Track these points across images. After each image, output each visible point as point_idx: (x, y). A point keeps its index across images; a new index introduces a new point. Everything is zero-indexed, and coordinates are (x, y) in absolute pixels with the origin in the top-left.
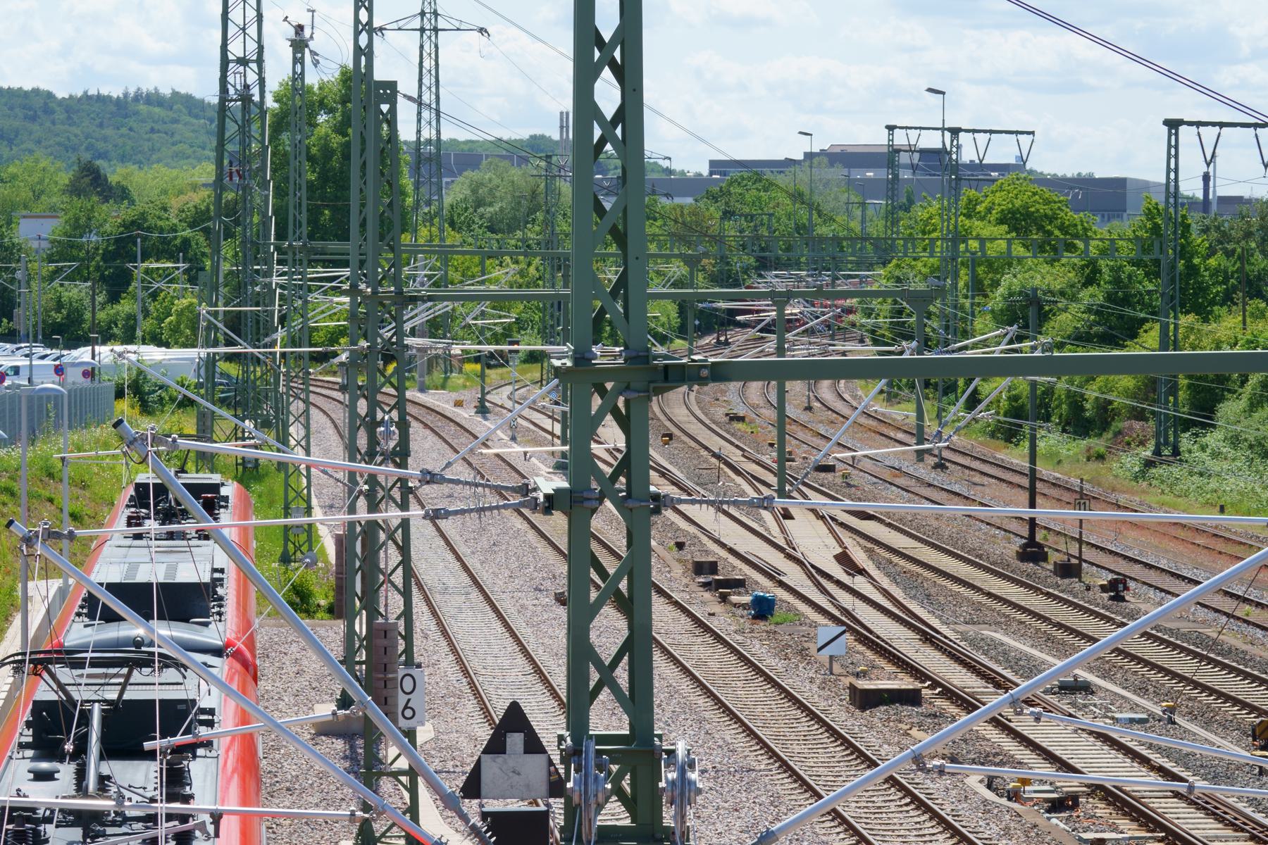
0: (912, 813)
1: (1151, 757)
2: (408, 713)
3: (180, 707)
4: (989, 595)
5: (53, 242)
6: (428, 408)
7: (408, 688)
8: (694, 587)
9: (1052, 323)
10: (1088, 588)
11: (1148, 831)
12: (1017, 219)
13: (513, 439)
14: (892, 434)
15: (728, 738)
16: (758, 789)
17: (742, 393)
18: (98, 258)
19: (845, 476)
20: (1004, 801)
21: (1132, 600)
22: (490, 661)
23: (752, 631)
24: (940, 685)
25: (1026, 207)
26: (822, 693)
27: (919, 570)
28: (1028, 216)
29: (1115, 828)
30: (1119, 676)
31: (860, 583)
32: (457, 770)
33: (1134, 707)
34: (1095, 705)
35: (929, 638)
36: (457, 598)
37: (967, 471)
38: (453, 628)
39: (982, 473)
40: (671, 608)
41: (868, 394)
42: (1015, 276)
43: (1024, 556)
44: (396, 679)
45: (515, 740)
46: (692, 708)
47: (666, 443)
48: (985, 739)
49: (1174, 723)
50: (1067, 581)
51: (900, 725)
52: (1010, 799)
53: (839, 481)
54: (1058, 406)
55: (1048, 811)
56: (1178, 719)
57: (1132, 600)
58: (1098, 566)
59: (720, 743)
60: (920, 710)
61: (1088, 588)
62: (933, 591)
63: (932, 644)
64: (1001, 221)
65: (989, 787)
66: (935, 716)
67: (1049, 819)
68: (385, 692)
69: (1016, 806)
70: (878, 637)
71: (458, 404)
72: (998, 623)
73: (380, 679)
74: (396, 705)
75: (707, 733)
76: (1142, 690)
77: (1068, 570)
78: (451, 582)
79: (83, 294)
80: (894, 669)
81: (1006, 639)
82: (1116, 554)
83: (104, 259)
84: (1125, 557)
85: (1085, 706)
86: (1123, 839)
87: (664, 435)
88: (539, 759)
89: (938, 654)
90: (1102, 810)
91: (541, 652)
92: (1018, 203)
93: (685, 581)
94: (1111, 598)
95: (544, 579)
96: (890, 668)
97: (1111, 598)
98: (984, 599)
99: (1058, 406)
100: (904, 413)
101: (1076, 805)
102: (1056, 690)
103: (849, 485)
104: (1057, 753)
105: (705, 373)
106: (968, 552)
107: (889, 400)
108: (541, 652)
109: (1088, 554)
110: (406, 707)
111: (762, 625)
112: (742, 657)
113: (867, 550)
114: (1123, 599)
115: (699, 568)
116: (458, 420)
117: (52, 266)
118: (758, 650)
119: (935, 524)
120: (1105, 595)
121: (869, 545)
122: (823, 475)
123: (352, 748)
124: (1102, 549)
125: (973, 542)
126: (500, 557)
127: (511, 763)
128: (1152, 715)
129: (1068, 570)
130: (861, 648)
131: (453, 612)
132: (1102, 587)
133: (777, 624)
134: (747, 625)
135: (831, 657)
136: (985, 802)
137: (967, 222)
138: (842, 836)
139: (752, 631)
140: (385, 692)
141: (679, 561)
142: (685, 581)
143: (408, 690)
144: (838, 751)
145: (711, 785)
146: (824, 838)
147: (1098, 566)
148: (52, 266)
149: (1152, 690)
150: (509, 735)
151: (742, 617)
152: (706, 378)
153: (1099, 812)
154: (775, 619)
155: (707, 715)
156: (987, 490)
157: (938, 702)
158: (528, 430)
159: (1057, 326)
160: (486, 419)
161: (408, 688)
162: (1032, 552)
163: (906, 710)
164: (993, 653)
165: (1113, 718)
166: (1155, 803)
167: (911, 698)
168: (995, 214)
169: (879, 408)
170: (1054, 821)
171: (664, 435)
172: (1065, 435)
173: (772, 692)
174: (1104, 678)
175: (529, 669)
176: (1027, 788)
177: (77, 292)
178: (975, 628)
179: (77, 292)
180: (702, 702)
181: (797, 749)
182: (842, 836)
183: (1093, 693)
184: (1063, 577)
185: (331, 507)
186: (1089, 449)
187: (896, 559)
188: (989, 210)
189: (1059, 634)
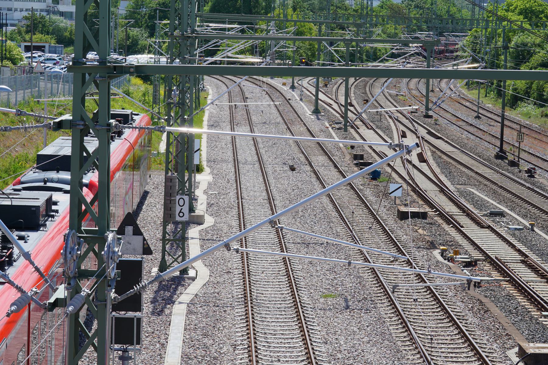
0: (404, 265)
1: (516, 245)
2: (181, 214)
3: (33, 209)
4: (476, 173)
5: (127, 11)
6: (271, 86)
7: (181, 204)
8: (352, 165)
9: (533, 58)
10: (520, 172)
11: (503, 277)
12: (527, 13)
13: (301, 100)
14: (464, 103)
15: (338, 230)
16: (342, 252)
17: (447, 84)
18: (147, 17)
19: (436, 120)
20: (446, 262)
21: (538, 177)
22: (252, 193)
23: (369, 185)
24: (439, 211)
25: (531, 7)
26: (387, 212)
27: (452, 161)
28: (532, 12)
29: (489, 275)
30: (518, 209)
31: (423, 167)
32: (217, 239)
33: (519, 223)
34: (503, 222)
35: (443, 190)
36: (249, 166)
37: (490, 120)
38: (243, 179)
39: (495, 121)
40: (338, 173)
41: (459, 84)
42: (519, 37)
43: (498, 157)
44: (175, 200)
45: (129, 229)
46: (328, 216)
47: (365, 104)
48: (449, 235)
49: (534, 231)
50: (513, 168)
51: (415, 227)
52: (449, 261)
53: (433, 122)
54: (533, 93)
55: (464, 267)
56: (535, 229)
57: (538, 177)
58: (528, 162)
59: (334, 232)
60: (425, 221)
61: (520, 172)
62: (453, 170)
63: (444, 193)
64: (520, 14)
65: (442, 256)
66: (431, 224)
67: (463, 270)
68: (170, 205)
69: (450, 264)
70: (420, 189)
71: (284, 84)
72: (475, 185)
73: (168, 200)
74: (175, 211)
75: (331, 228)
76: (524, 216)
77: (513, 164)
78: (249, 159)
79: (138, 33)
80: (423, 203)
81: (475, 192)
82: (539, 157)
83: (149, 18)
84: (542, 159)
85: (498, 222)
86: (491, 280)
87: (365, 100)
88: (140, 238)
89: (444, 197)
90: (487, 267)
91: (274, 190)
92: (528, 6)
93: (349, 162)
94: (529, 176)
95: (289, 159)
96: (421, 202)
97: (529, 176)
98: (473, 174)
99: (533, 93)
100: (472, 94)
101: (476, 265)
102: (489, 214)
103: (436, 124)
104: (476, 242)
105: (132, 70)
106: (475, 155)
107: (468, 88)
108: (274, 190)
109: (523, 155)
110: (180, 212)
111: (374, 182)
112: (359, 196)
113: (433, 153)
114: (533, 177)
115: (356, 157)
116: (281, 91)
117: (127, 21)
118: (369, 194)
119: (466, 141)
120: (527, 175)
121: (434, 150)
122: (427, 119)
123: (176, 228)
124: (534, 155)
125: (479, 150)
126: (274, 150)
127: (127, 239)
128: (525, 227)
129: (513, 164)
130: (412, 193)
131: (245, 171)
132: (526, 171)
133: (381, 182)
134: (368, 182)
135: (395, 197)
136: (438, 262)
137: (506, 13)
138: (370, 274)
139: (369, 185)
140: (170, 205)
141: (350, 154)
142: (349, 162)
143: (181, 205)
144: (384, 237)
145: (322, 250)
146: (361, 275)
147: (528, 162)
148: (127, 21)
149: (529, 216)
150: (126, 227)
151: (367, 178)
152: (133, 73)
153: (485, 268)
154: (379, 180)
155: (334, 220)
156: (494, 128)
157: (436, 218)
158: (309, 96)
159: (535, 59)
160: (293, 91)
161: (181, 204)
162: (501, 155)
163: (419, 221)
164: (468, 198)
165: (508, 228)
166: (511, 266)
167: (424, 216)
168: (517, 11)
169: (465, 91)
170: (465, 271)
171: (365, 100)
172: (535, 106)
173: (366, 211)
174: (511, 210)
175: (266, 197)
176: (457, 256)
177: (135, 32)
178: (465, 186)
179: (135, 32)
180: (334, 214)
181: (367, 235)
182: (370, 274)
183: (504, 216)
184: (511, 166)
185: (212, 126)
186: (543, 112)
187: (444, 157)
188: (516, 8)
189: (500, 191)
